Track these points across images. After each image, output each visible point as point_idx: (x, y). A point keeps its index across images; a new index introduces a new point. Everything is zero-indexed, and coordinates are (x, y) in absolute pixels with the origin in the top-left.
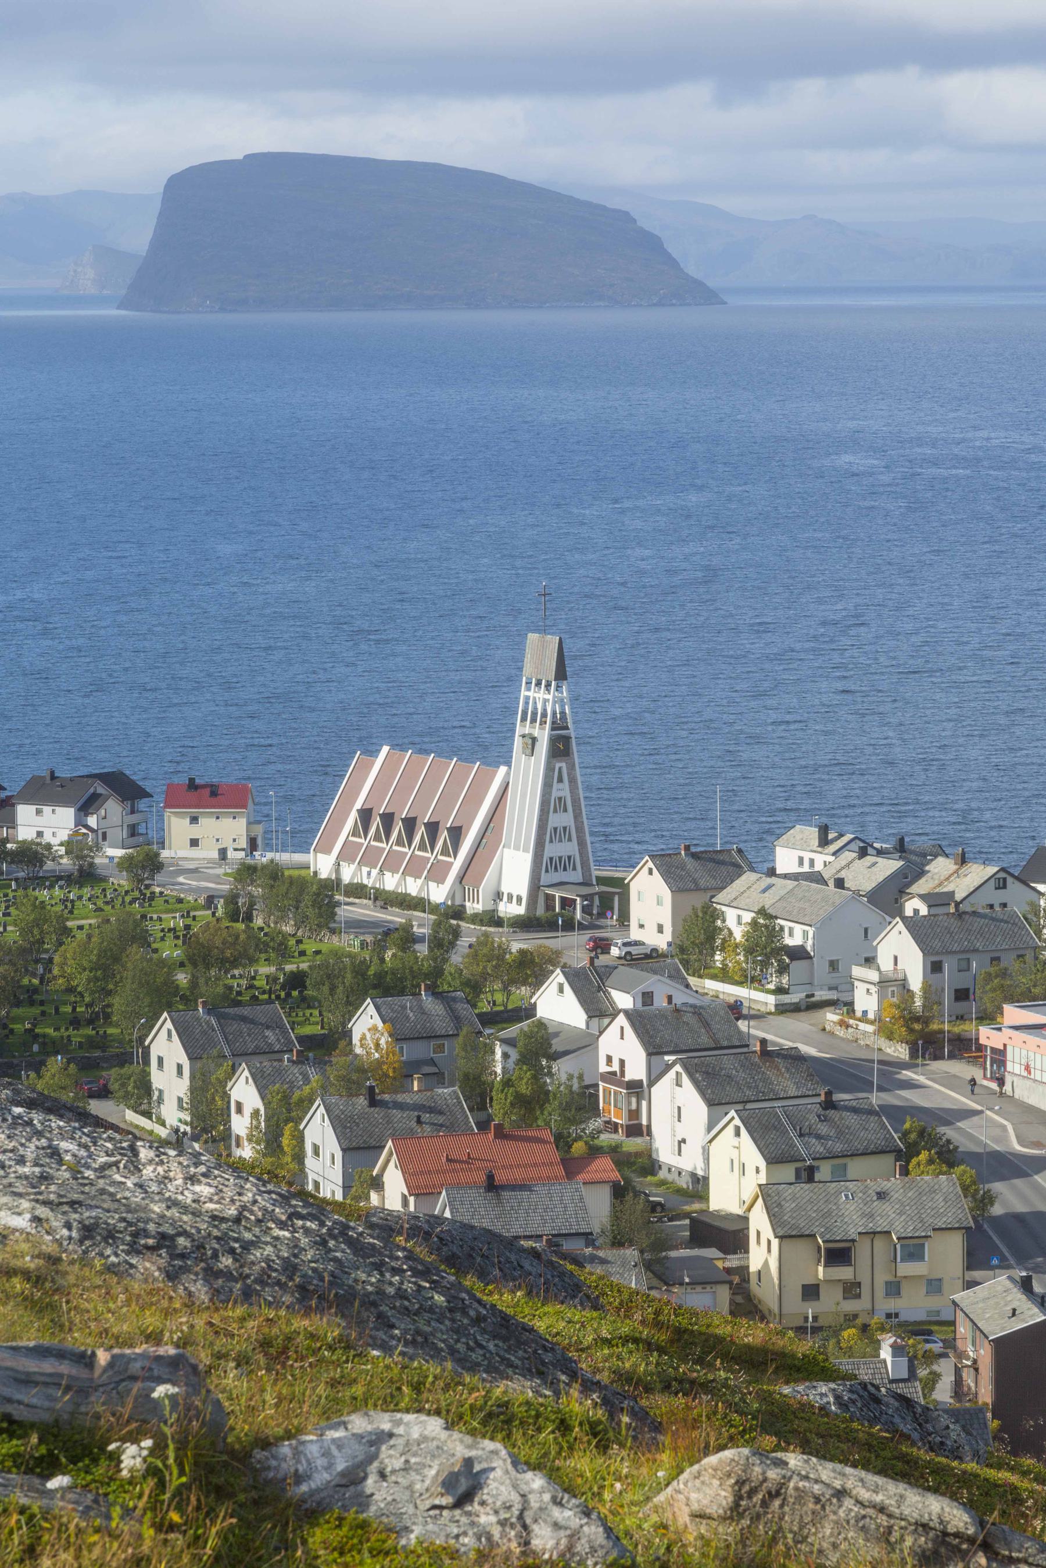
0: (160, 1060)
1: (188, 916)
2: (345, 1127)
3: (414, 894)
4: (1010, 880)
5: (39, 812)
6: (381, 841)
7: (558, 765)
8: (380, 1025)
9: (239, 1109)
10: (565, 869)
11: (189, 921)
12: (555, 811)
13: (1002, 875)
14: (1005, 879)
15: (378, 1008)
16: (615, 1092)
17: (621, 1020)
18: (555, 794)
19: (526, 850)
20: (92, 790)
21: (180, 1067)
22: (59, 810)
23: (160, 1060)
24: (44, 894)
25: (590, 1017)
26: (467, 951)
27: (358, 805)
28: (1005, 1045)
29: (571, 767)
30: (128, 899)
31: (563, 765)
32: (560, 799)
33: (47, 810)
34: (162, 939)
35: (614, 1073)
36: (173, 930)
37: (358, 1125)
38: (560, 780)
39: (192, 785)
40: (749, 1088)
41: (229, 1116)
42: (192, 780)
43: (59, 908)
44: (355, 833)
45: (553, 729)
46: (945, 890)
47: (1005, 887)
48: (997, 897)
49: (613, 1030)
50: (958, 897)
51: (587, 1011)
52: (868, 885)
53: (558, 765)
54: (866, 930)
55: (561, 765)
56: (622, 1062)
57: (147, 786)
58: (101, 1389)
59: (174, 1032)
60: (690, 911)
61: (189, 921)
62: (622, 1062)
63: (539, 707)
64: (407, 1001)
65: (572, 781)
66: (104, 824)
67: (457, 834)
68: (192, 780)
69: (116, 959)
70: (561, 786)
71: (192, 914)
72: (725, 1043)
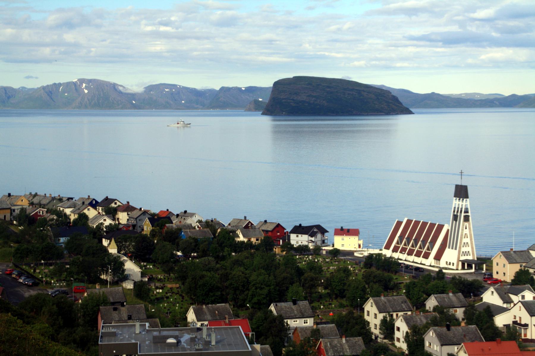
0: (368, 312)
3: (125, 268)
5: (297, 236)
9: (398, 329)
15: (435, 298)
19: (456, 249)
21: (368, 315)
22: (303, 235)
23: (368, 312)
27: (414, 238)
29: (469, 225)
33: (300, 235)
38: (466, 228)
39: (342, 229)
42: (342, 227)
51: (503, 300)
56: (520, 318)
57: (328, 230)
58: (19, 269)
59: (373, 304)
62: (520, 318)
63: (460, 207)
64: (444, 295)
65: (470, 229)
66: (316, 240)
68: (342, 227)
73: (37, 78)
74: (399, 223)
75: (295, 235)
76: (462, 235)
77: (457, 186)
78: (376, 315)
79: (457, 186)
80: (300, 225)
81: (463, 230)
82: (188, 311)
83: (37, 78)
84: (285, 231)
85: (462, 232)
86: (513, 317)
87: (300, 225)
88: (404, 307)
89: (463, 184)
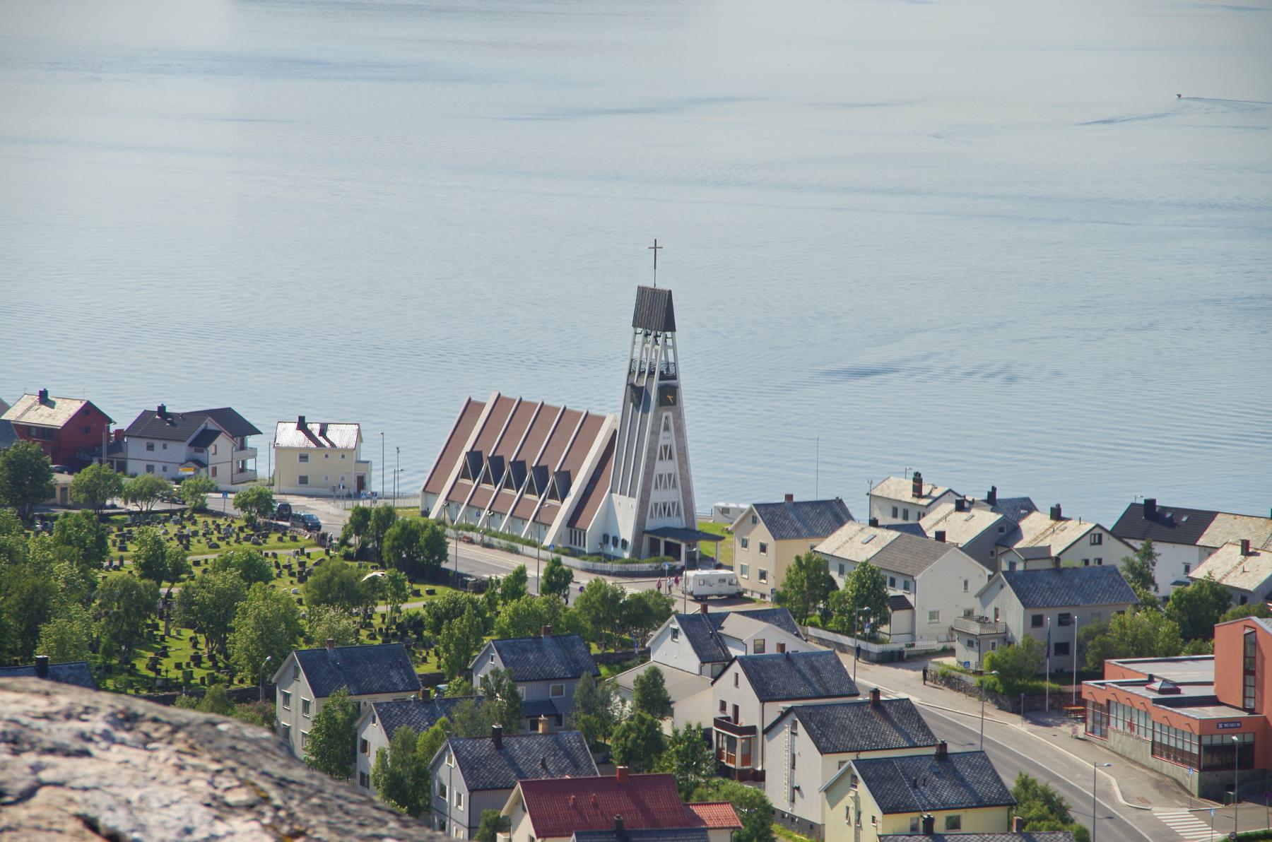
1: (302, 553)
2: (472, 769)
4: (1105, 536)
6: (534, 493)
7: (665, 414)
8: (502, 668)
10: (669, 514)
11: (303, 559)
12: (661, 458)
13: (1098, 531)
14: (1100, 536)
16: (718, 733)
17: (736, 667)
18: (662, 442)
19: (632, 495)
20: (202, 426)
22: (170, 445)
24: (158, 530)
25: (703, 663)
26: (579, 594)
27: (467, 448)
28: (1108, 702)
30: (242, 535)
31: (670, 414)
32: (666, 448)
33: (158, 445)
34: (279, 575)
35: (728, 719)
36: (288, 567)
37: (484, 766)
38: (667, 428)
40: (862, 737)
41: (355, 753)
43: (175, 543)
44: (464, 474)
45: (660, 379)
46: (1041, 544)
47: (1100, 543)
48: (1093, 553)
49: (729, 676)
50: (1054, 553)
51: (700, 657)
52: (964, 540)
53: (665, 414)
54: (966, 583)
55: (668, 413)
56: (736, 708)
60: (793, 561)
61: (303, 559)
62: (736, 708)
67: (566, 480)
69: (576, 661)
70: (667, 434)
71: (306, 551)
72: (836, 692)
73: (656, 312)
74: (471, 408)
75: (143, 443)
76: (651, 451)
77: (642, 291)
78: (306, 704)
79: (642, 291)
80: (162, 409)
81: (655, 433)
82: (903, 812)
83: (656, 312)
84: (113, 428)
85: (653, 443)
86: (718, 707)
87: (162, 409)
88: (396, 679)
89: (661, 286)
